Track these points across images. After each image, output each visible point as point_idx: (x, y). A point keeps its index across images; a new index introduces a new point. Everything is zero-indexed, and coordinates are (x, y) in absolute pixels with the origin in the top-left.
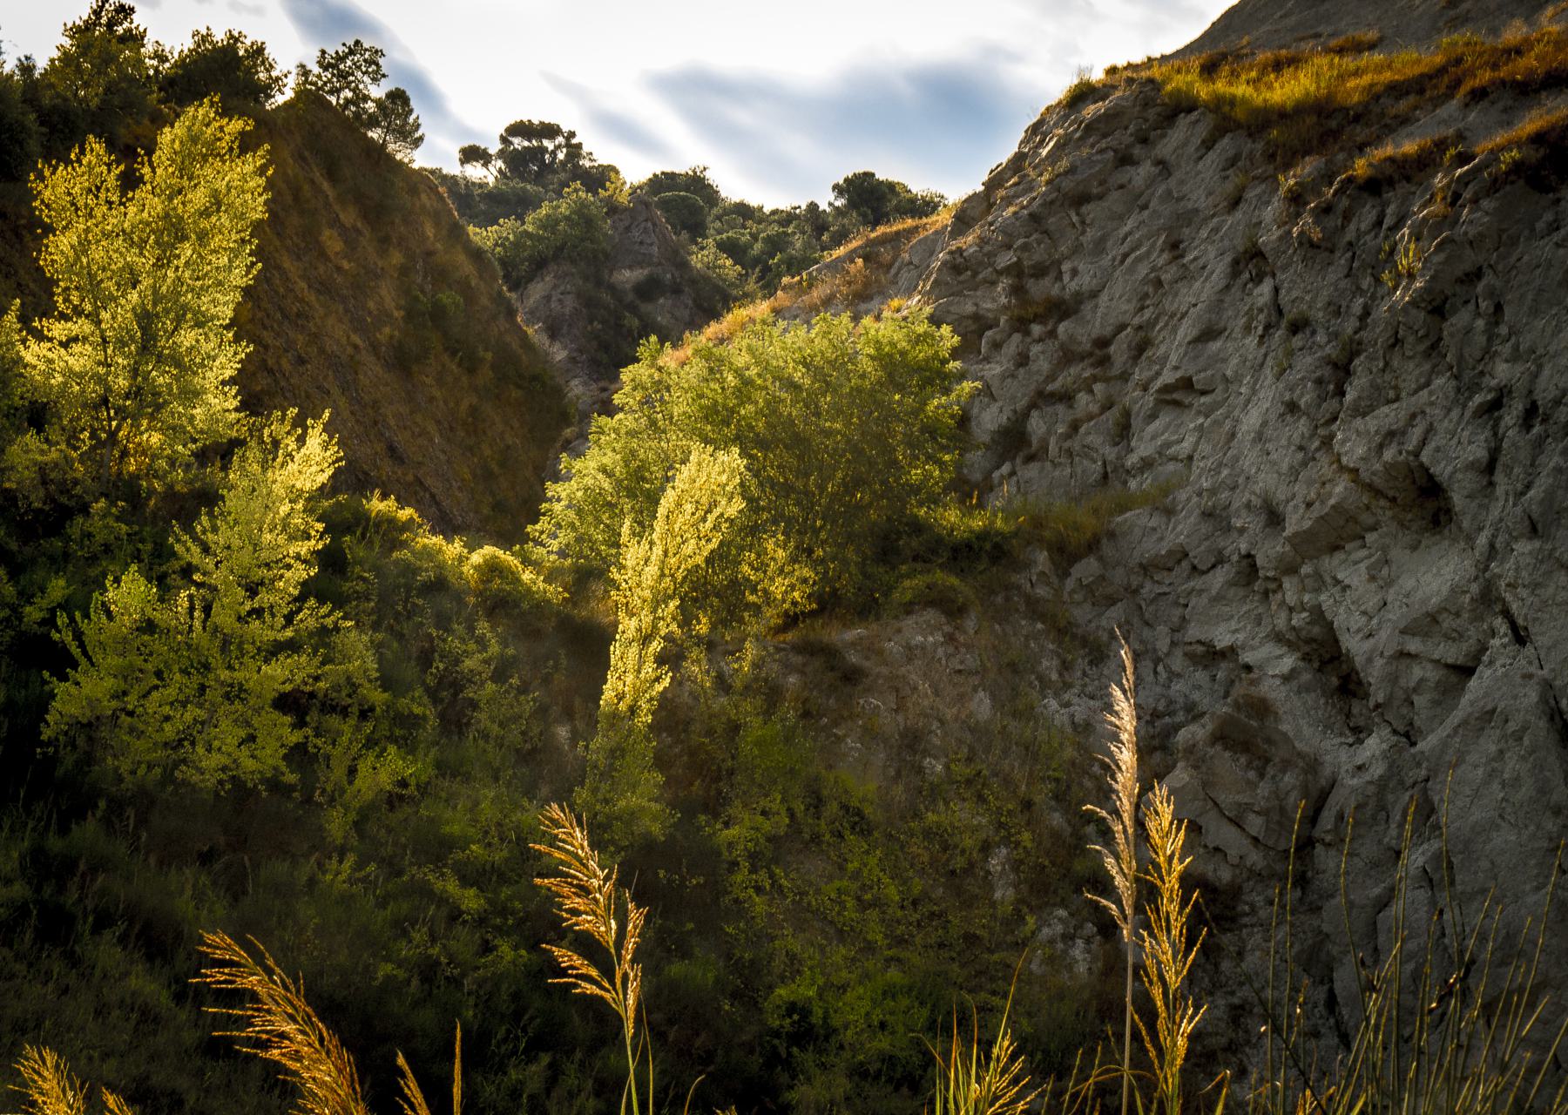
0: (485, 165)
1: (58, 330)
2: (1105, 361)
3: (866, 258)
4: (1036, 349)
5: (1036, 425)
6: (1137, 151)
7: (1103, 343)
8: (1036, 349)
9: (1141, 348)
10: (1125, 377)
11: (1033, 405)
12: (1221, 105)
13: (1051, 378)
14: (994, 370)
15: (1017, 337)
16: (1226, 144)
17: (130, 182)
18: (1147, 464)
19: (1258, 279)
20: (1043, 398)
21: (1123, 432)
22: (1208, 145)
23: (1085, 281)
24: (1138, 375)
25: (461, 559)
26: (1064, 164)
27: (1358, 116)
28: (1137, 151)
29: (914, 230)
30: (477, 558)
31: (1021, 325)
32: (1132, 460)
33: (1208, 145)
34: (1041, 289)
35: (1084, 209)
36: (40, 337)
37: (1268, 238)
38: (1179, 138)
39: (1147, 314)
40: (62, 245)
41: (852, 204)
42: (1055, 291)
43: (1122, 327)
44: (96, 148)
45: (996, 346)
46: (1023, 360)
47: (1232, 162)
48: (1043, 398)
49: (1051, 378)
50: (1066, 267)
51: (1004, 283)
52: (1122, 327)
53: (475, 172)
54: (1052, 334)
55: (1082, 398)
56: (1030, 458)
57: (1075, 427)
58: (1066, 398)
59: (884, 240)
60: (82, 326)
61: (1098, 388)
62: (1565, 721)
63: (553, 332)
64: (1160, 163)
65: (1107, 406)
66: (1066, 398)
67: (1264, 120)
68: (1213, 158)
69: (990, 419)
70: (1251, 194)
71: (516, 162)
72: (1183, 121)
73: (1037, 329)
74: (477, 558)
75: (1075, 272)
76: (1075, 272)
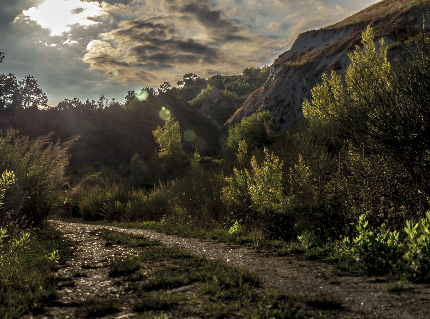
0: (182, 84)
1: (162, 150)
2: (290, 107)
3: (253, 97)
4: (280, 108)
5: (284, 118)
6: (286, 76)
7: (289, 104)
8: (280, 108)
9: (294, 104)
10: (293, 108)
11: (282, 116)
12: (295, 67)
13: (284, 111)
14: (276, 112)
15: (277, 107)
16: (297, 72)
17: (163, 130)
18: (299, 119)
19: (306, 91)
20: (283, 114)
21: (295, 116)
22: (295, 72)
23: (284, 96)
24: (295, 108)
25: (219, 161)
26: (276, 81)
27: (313, 63)
28: (286, 76)
29: (259, 91)
30: (220, 161)
31: (278, 105)
32: (297, 119)
33: (295, 72)
34: (278, 99)
35: (281, 86)
36: (160, 152)
37: (305, 86)
38: (291, 72)
39: (293, 99)
40: (158, 140)
41: (246, 74)
42: (281, 99)
43: (291, 101)
44: (159, 127)
45: (275, 109)
46: (279, 110)
47: (298, 74)
48: (283, 114)
49: (284, 111)
50: (281, 95)
51: (274, 100)
52: (291, 101)
53: (182, 86)
54: (282, 105)
55: (288, 112)
56: (284, 123)
57: (289, 117)
58: (286, 113)
59: (255, 93)
60: (164, 149)
61: (290, 110)
62: (18, 318)
63: (207, 114)
64: (289, 77)
65: (292, 113)
66: (286, 113)
67: (301, 67)
68: (296, 74)
69: (277, 119)
70: (302, 79)
71: (189, 82)
72: (291, 70)
73: (280, 105)
74: (220, 161)
75: (282, 95)
76: (282, 95)
